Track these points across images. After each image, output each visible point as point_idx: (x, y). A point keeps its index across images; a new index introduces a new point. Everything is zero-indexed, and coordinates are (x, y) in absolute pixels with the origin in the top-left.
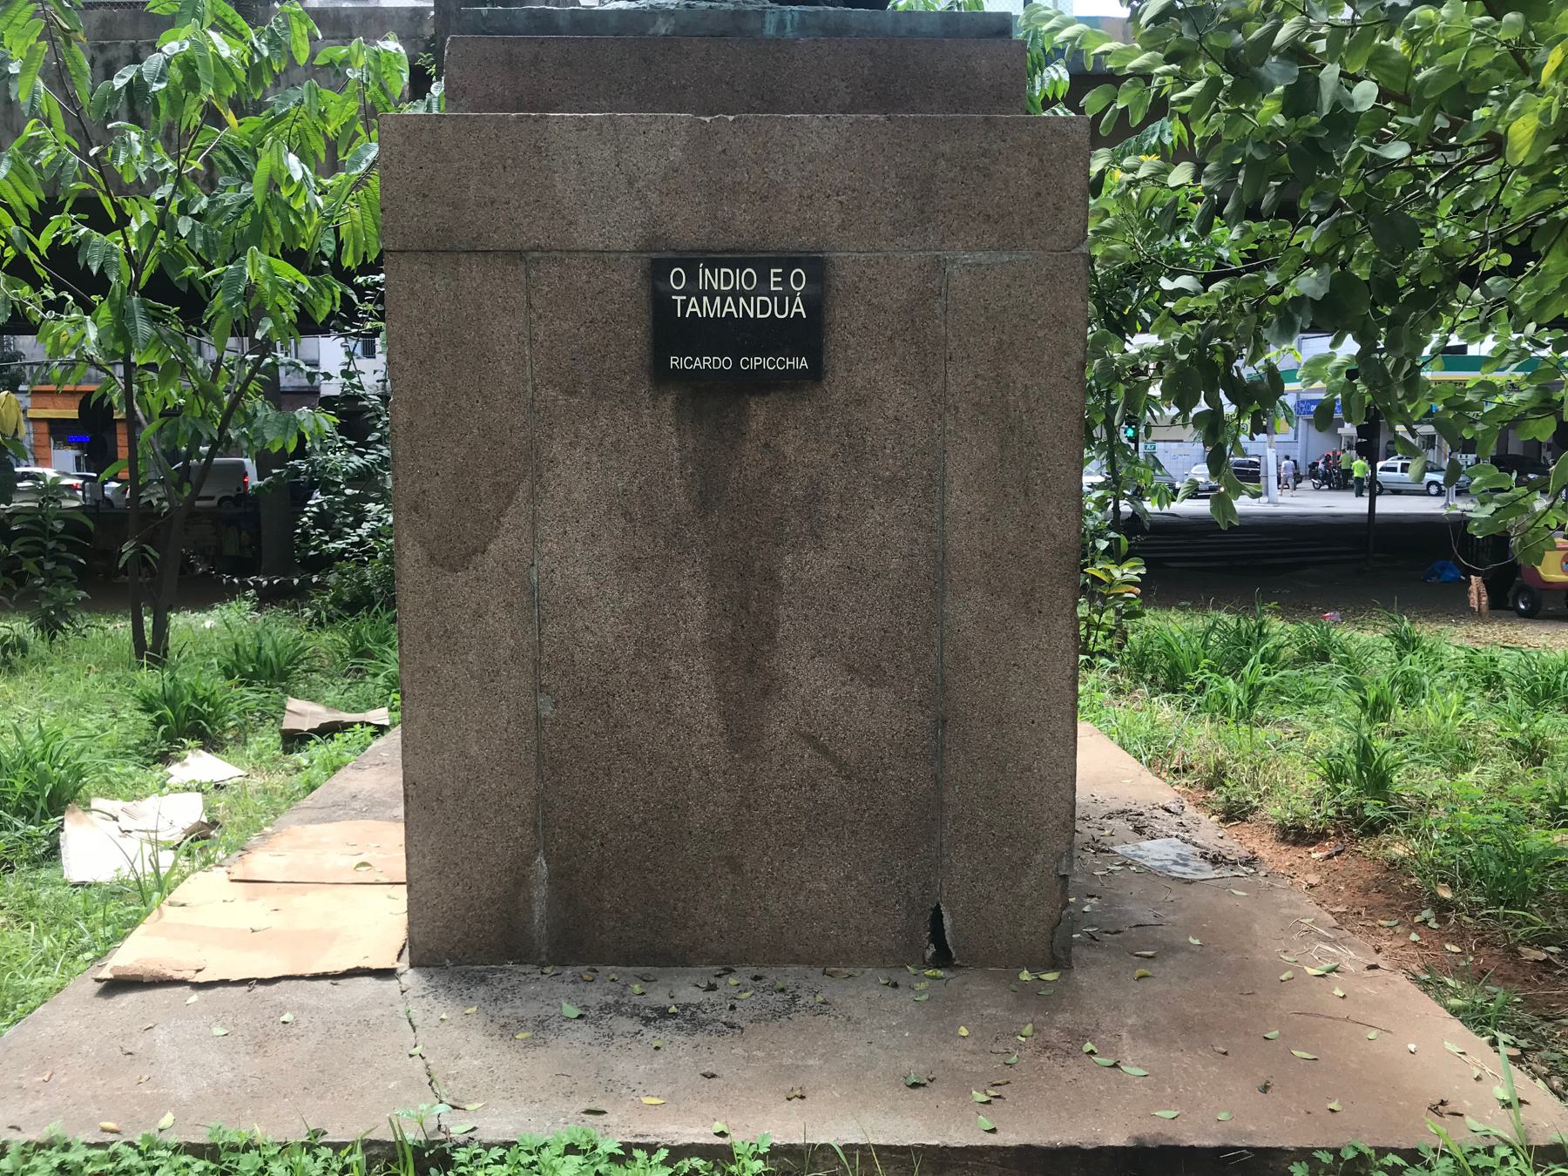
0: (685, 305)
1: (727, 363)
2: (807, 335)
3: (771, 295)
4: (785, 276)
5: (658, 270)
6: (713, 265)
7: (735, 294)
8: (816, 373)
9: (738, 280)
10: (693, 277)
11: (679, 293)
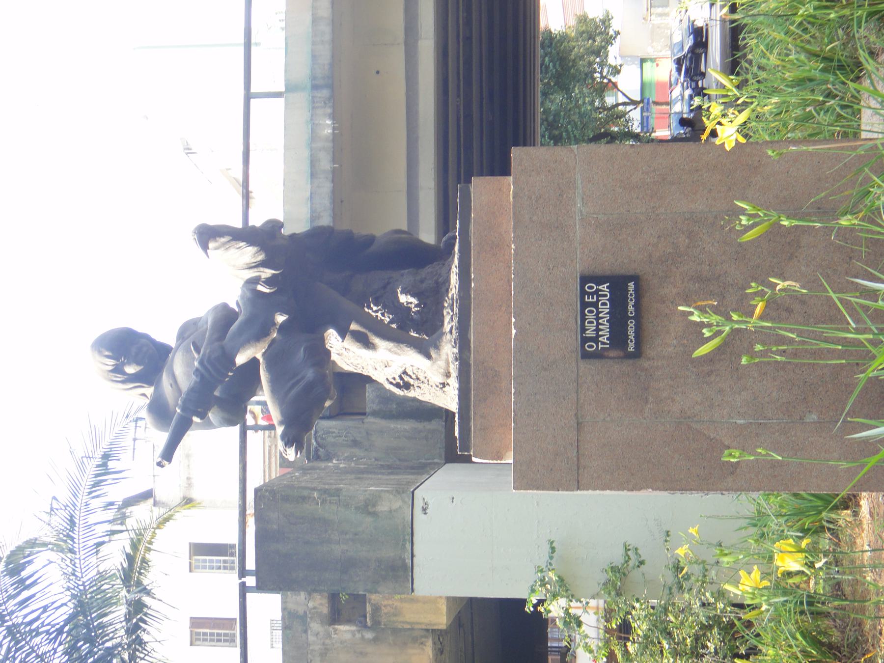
0: (603, 343)
1: (631, 313)
2: (618, 283)
3: (598, 301)
4: (589, 294)
5: (586, 355)
6: (583, 330)
7: (598, 319)
8: (636, 279)
9: (590, 317)
10: (591, 339)
11: (597, 346)
